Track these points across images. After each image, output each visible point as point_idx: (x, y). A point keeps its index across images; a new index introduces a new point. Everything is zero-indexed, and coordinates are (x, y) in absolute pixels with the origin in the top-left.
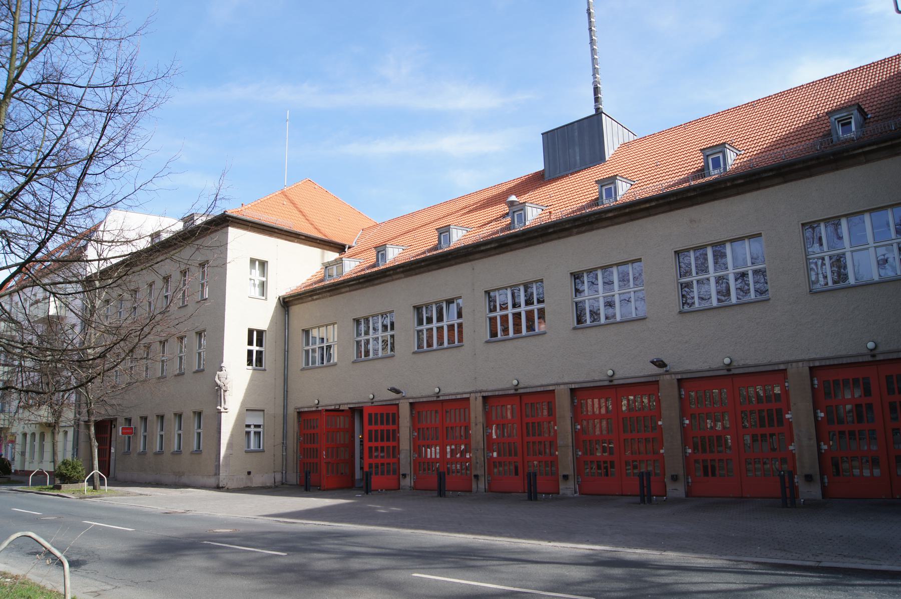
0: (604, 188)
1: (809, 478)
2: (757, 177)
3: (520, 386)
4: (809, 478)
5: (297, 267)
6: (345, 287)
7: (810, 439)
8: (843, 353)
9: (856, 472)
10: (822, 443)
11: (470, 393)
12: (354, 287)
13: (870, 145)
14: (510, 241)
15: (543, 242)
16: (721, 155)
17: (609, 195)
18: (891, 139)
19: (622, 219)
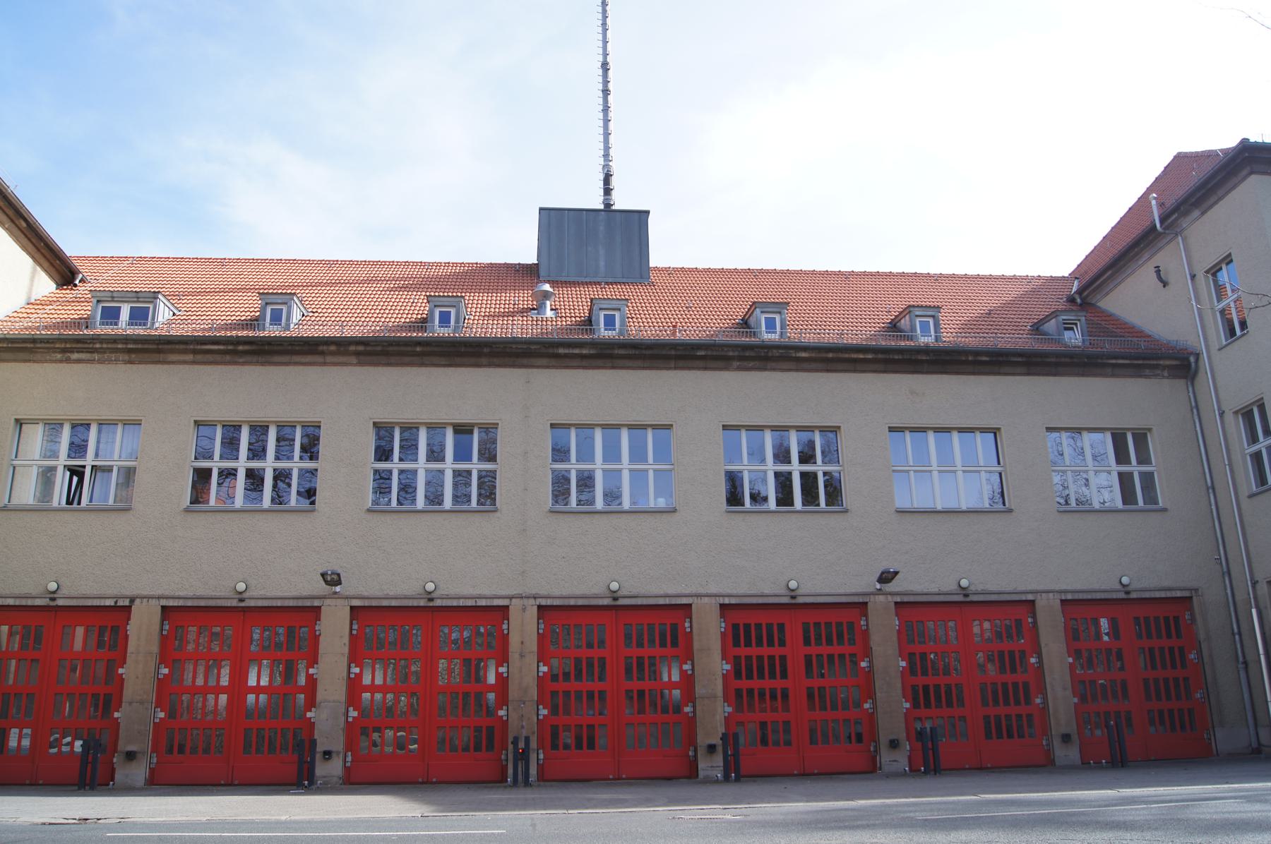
0: (101, 305)
1: (1066, 738)
3: (620, 594)
4: (1066, 738)
6: (185, 352)
7: (1065, 689)
8: (1096, 586)
10: (351, 709)
11: (511, 598)
12: (210, 357)
13: (1123, 358)
14: (622, 352)
17: (445, 319)
18: (1144, 359)
19: (814, 365)
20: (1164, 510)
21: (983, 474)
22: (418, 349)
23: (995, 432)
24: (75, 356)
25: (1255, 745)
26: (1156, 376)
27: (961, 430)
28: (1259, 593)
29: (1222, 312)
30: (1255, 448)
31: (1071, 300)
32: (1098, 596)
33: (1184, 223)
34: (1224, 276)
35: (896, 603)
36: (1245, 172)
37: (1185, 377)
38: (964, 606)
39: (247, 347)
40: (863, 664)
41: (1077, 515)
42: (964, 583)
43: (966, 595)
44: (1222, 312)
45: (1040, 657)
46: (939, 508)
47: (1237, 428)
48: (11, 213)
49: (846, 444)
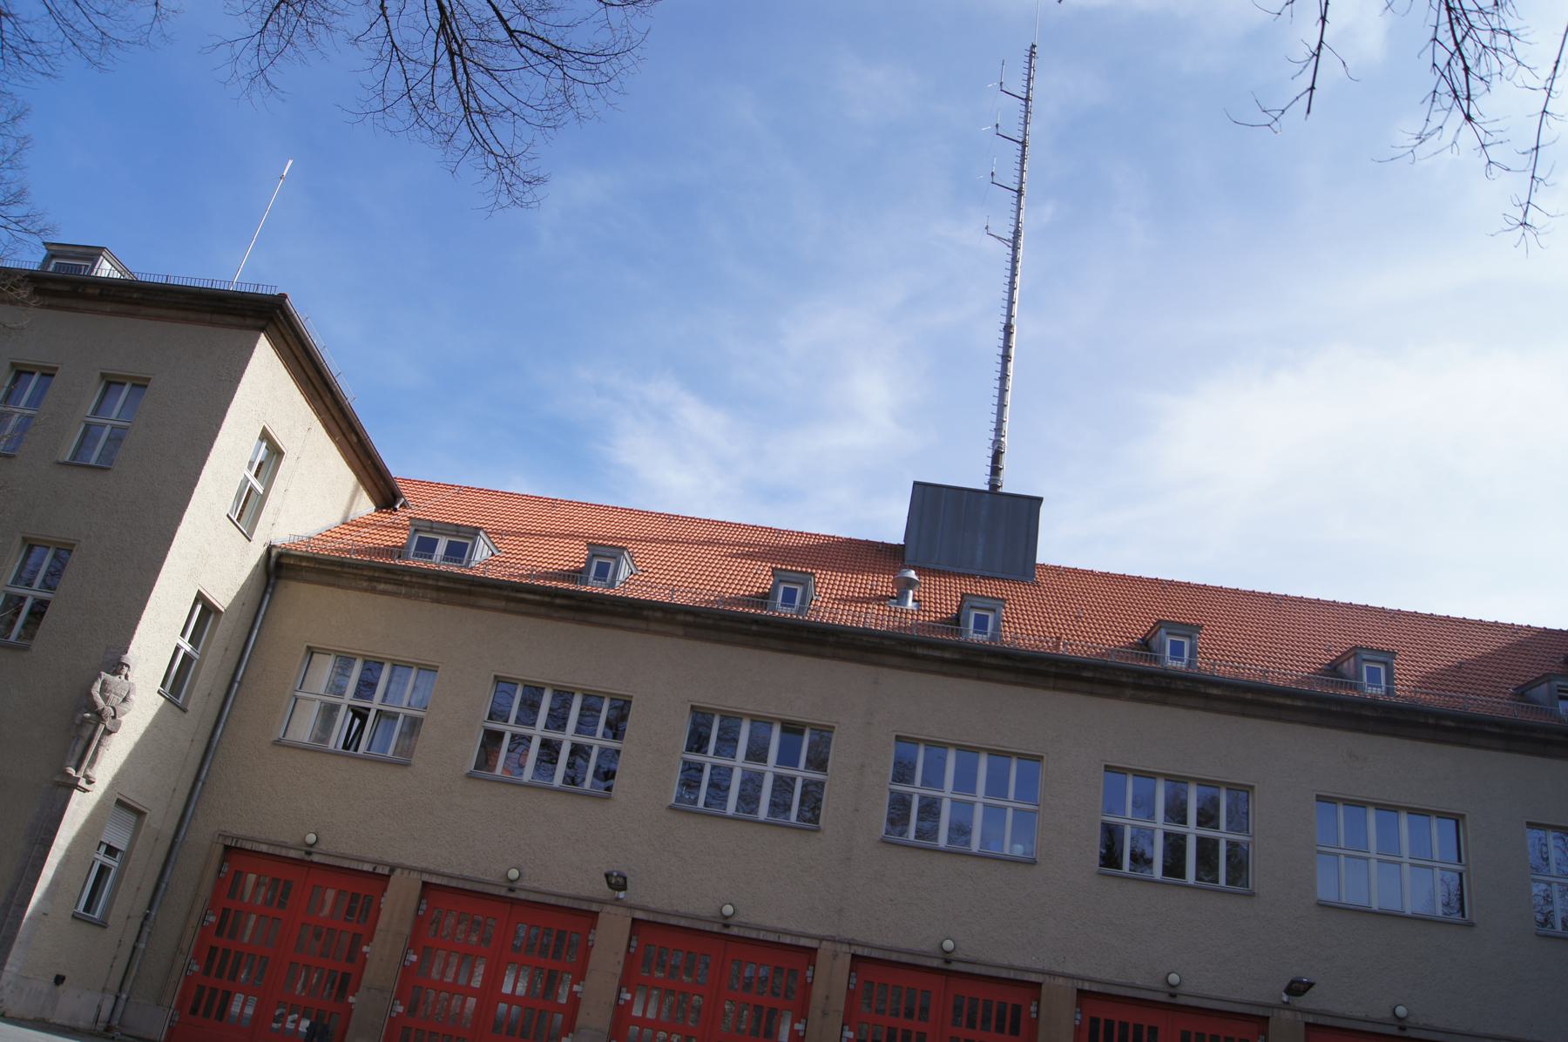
3: (518, 884)
5: (317, 500)
6: (498, 597)
11: (821, 939)
15: (1054, 689)
16: (613, 563)
17: (789, 597)
22: (754, 628)
23: (1458, 819)
24: (382, 586)
35: (1307, 1024)
39: (565, 602)
43: (1402, 1028)
46: (1375, 907)
48: (344, 426)
49: (836, 756)
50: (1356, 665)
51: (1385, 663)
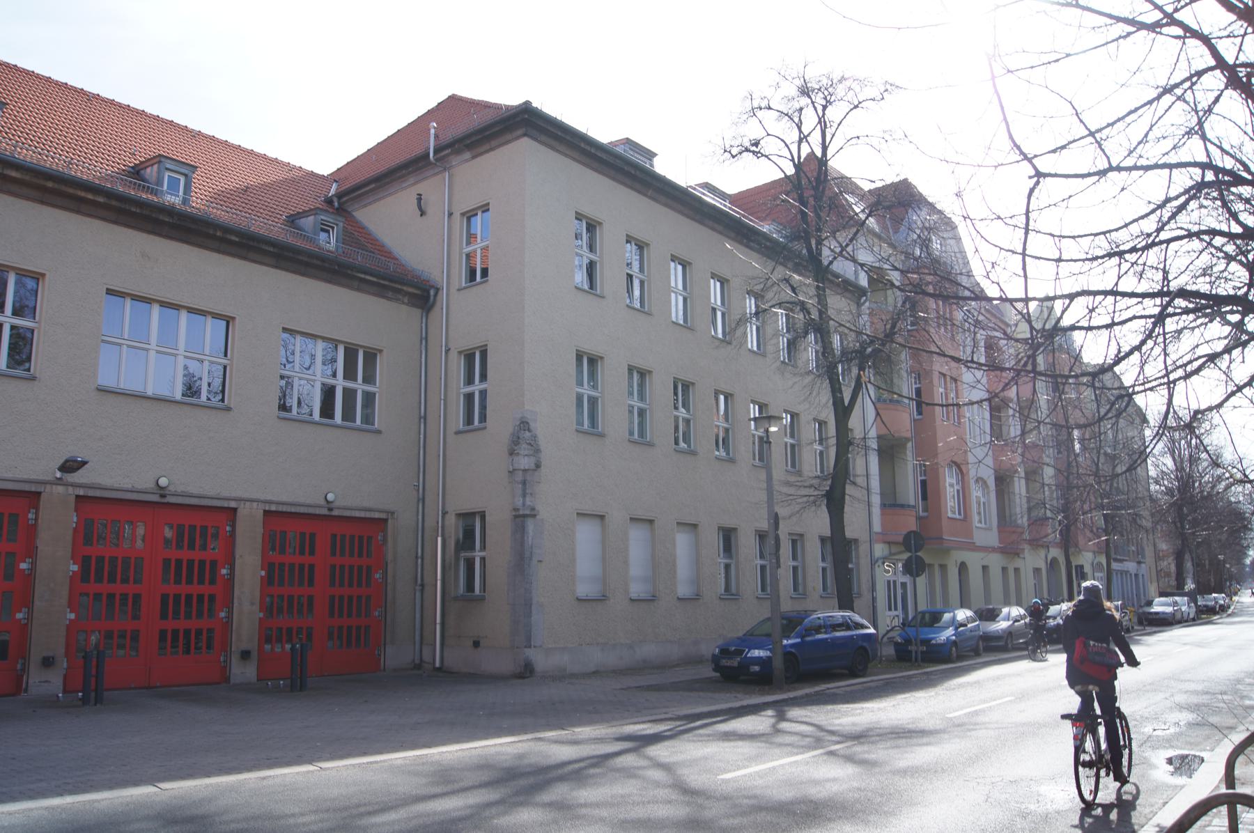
2: (255, 244)
4: (245, 655)
7: (252, 604)
8: (302, 500)
9: (278, 649)
13: (371, 275)
18: (391, 281)
20: (379, 432)
21: (206, 363)
23: (229, 320)
25: (417, 661)
26: (397, 300)
27: (191, 310)
28: (447, 523)
29: (468, 256)
30: (469, 389)
31: (329, 201)
32: (302, 510)
33: (455, 160)
34: (478, 220)
35: (77, 496)
36: (519, 132)
37: (422, 308)
38: (157, 507)
40: (23, 566)
41: (297, 424)
42: (163, 482)
43: (330, 509)
44: (468, 256)
45: (232, 569)
46: (150, 393)
47: (458, 367)
49: (46, 301)
50: (159, 172)
51: (186, 175)
